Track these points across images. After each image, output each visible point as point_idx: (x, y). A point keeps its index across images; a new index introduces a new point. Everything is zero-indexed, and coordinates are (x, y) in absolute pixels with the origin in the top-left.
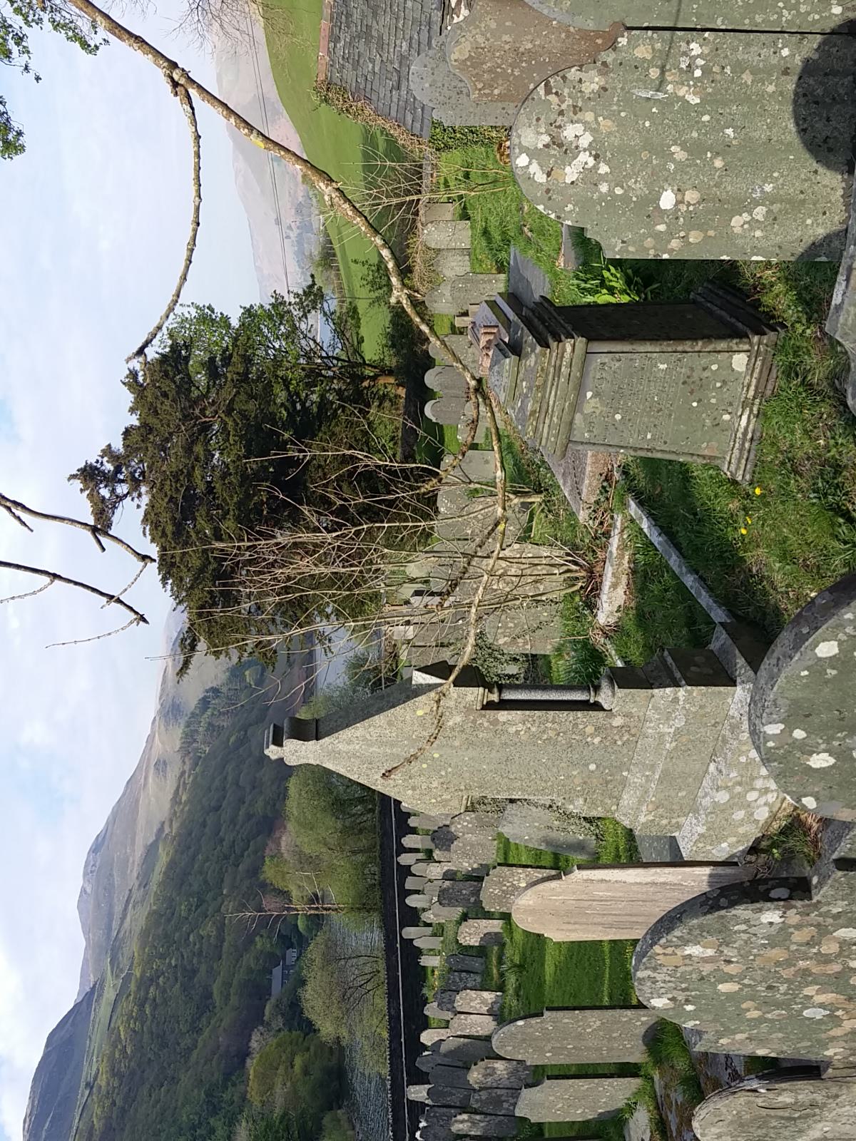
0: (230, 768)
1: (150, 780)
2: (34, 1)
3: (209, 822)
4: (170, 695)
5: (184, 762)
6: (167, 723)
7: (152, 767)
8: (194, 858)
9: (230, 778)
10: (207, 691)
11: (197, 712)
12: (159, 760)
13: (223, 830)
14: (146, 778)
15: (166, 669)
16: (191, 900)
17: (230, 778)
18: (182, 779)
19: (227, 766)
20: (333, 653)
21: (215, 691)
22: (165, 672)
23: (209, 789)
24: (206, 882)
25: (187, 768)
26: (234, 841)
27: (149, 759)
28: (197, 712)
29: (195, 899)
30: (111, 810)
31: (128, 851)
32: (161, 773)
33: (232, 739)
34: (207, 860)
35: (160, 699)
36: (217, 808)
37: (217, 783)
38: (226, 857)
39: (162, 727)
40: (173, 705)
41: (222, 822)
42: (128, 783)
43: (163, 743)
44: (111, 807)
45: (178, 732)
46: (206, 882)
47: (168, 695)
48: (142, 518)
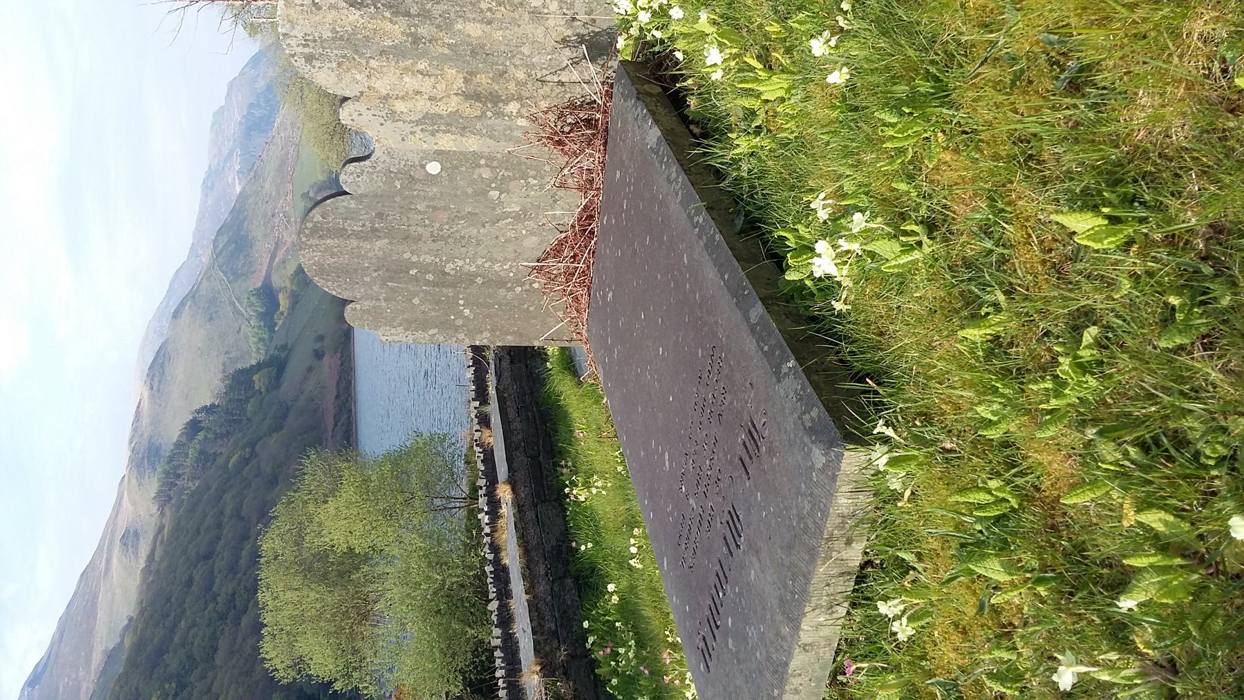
0: (228, 497)
1: (115, 561)
2: (765, 699)
3: (197, 578)
4: (145, 436)
5: (163, 514)
6: (141, 475)
7: (118, 542)
8: (175, 625)
9: (228, 512)
10: (198, 412)
11: (184, 440)
12: (127, 531)
13: (217, 581)
14: (108, 561)
15: (139, 403)
16: (167, 686)
17: (228, 512)
18: (160, 537)
19: (225, 496)
20: (476, 431)
21: (209, 410)
22: (138, 407)
23: (198, 532)
24: (190, 657)
25: (167, 521)
26: (233, 595)
27: (113, 532)
28: (184, 440)
29: (174, 685)
30: (56, 625)
31: (81, 674)
32: (130, 550)
33: (234, 459)
34: (194, 624)
35: (131, 442)
36: (208, 556)
37: (209, 520)
38: (222, 617)
39: (134, 481)
40: (149, 449)
41: (216, 573)
42: (82, 575)
43: (134, 503)
44: (192, 233)
45: (153, 486)
46: (190, 657)
47: (142, 435)
48: (225, 94)
